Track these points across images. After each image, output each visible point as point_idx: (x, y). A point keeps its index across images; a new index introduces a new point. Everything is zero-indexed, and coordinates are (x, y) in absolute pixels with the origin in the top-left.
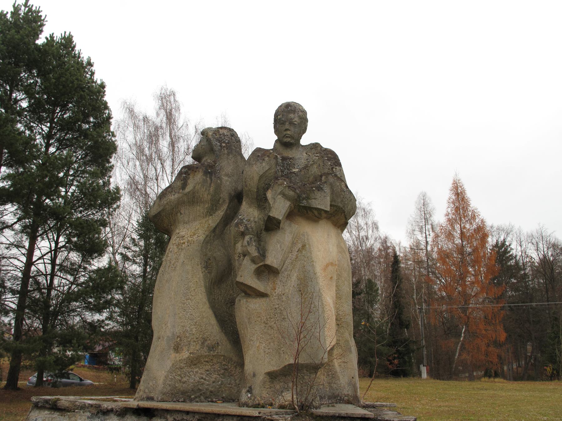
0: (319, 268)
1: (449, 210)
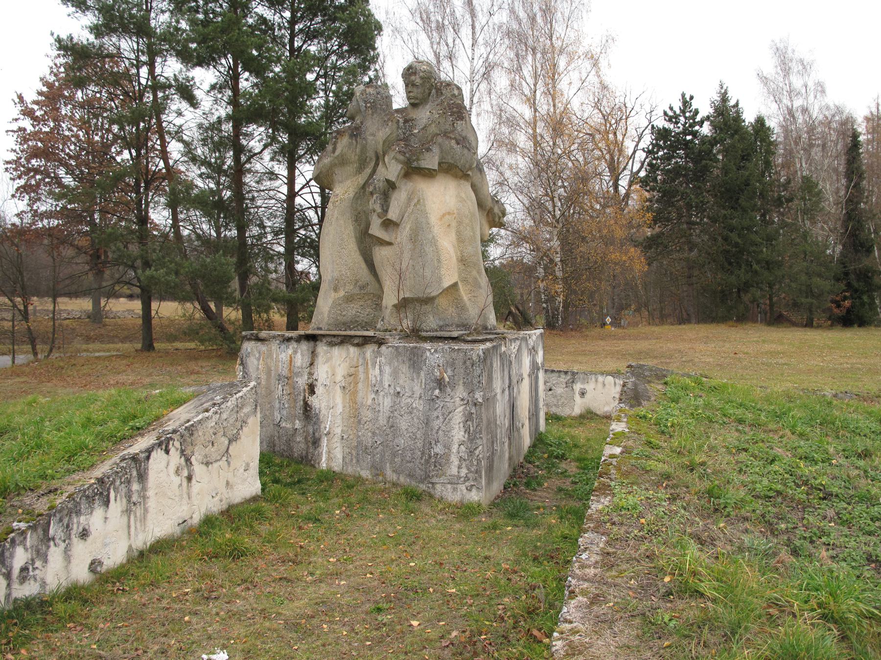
0: (433, 219)
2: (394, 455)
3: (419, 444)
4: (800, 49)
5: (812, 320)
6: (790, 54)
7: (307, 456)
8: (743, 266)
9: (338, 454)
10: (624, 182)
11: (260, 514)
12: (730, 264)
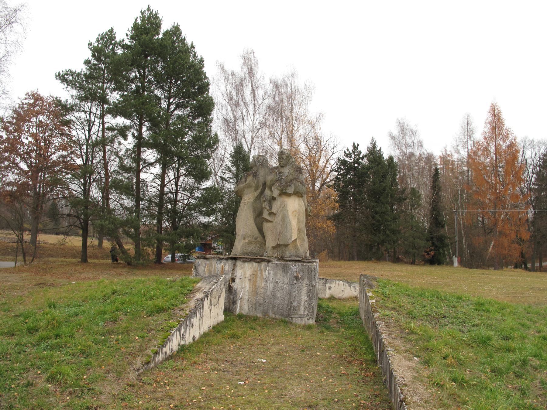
0: (290, 213)
1: (486, 130)
2: (274, 307)
3: (286, 302)
4: (411, 124)
5: (415, 261)
6: (406, 126)
7: (229, 309)
8: (382, 232)
9: (246, 307)
10: (318, 184)
11: (224, 327)
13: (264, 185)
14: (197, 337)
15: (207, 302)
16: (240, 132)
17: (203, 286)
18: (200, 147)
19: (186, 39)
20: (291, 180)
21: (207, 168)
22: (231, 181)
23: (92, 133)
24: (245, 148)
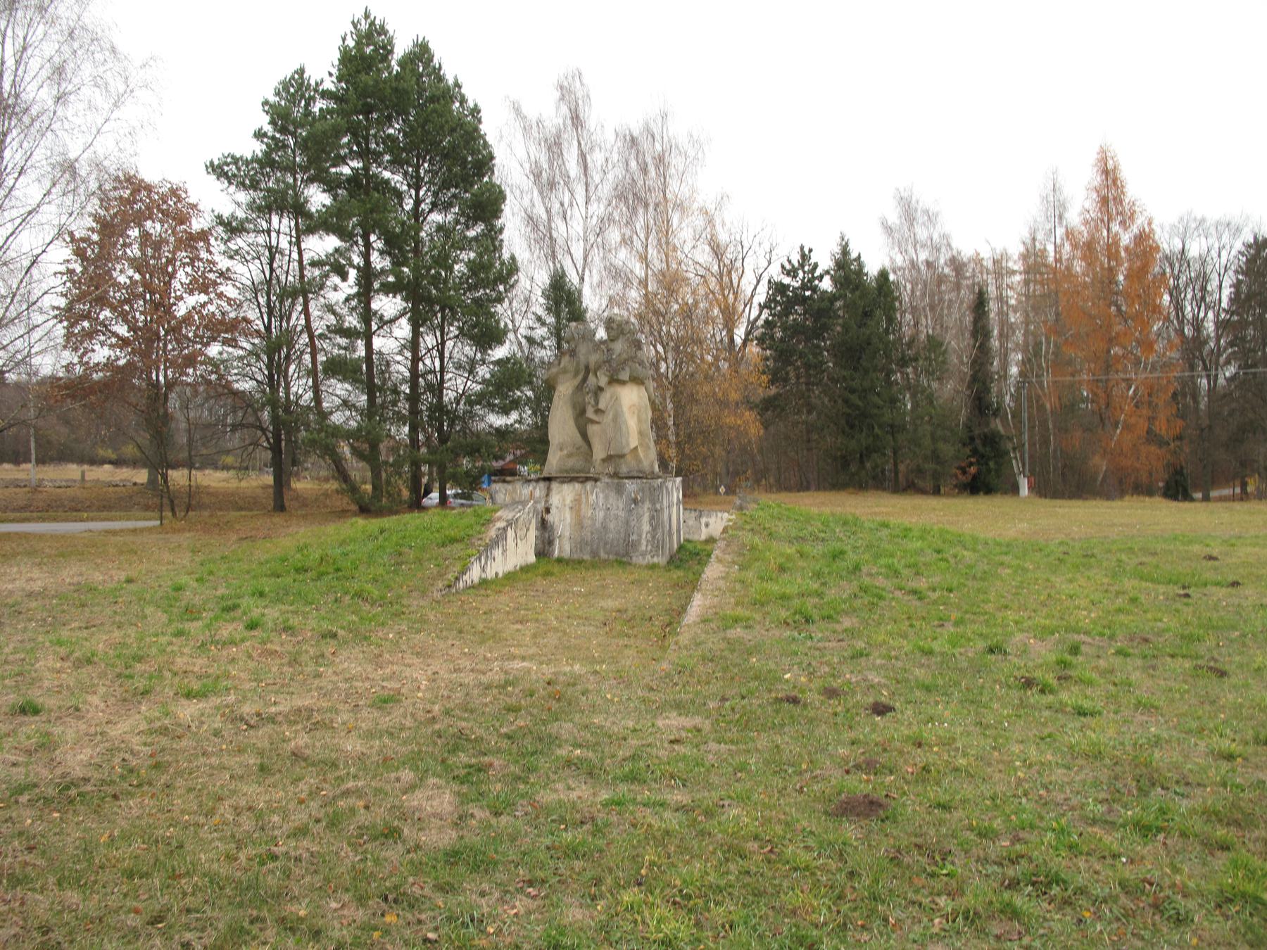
0: (625, 409)
2: (606, 544)
3: (622, 535)
4: (925, 199)
9: (567, 548)
12: (852, 427)
13: (587, 368)
14: (500, 575)
15: (510, 533)
16: (560, 241)
17: (506, 514)
18: (484, 284)
19: (444, 67)
20: (626, 361)
21: (498, 322)
22: (546, 343)
23: (275, 265)
24: (572, 277)
